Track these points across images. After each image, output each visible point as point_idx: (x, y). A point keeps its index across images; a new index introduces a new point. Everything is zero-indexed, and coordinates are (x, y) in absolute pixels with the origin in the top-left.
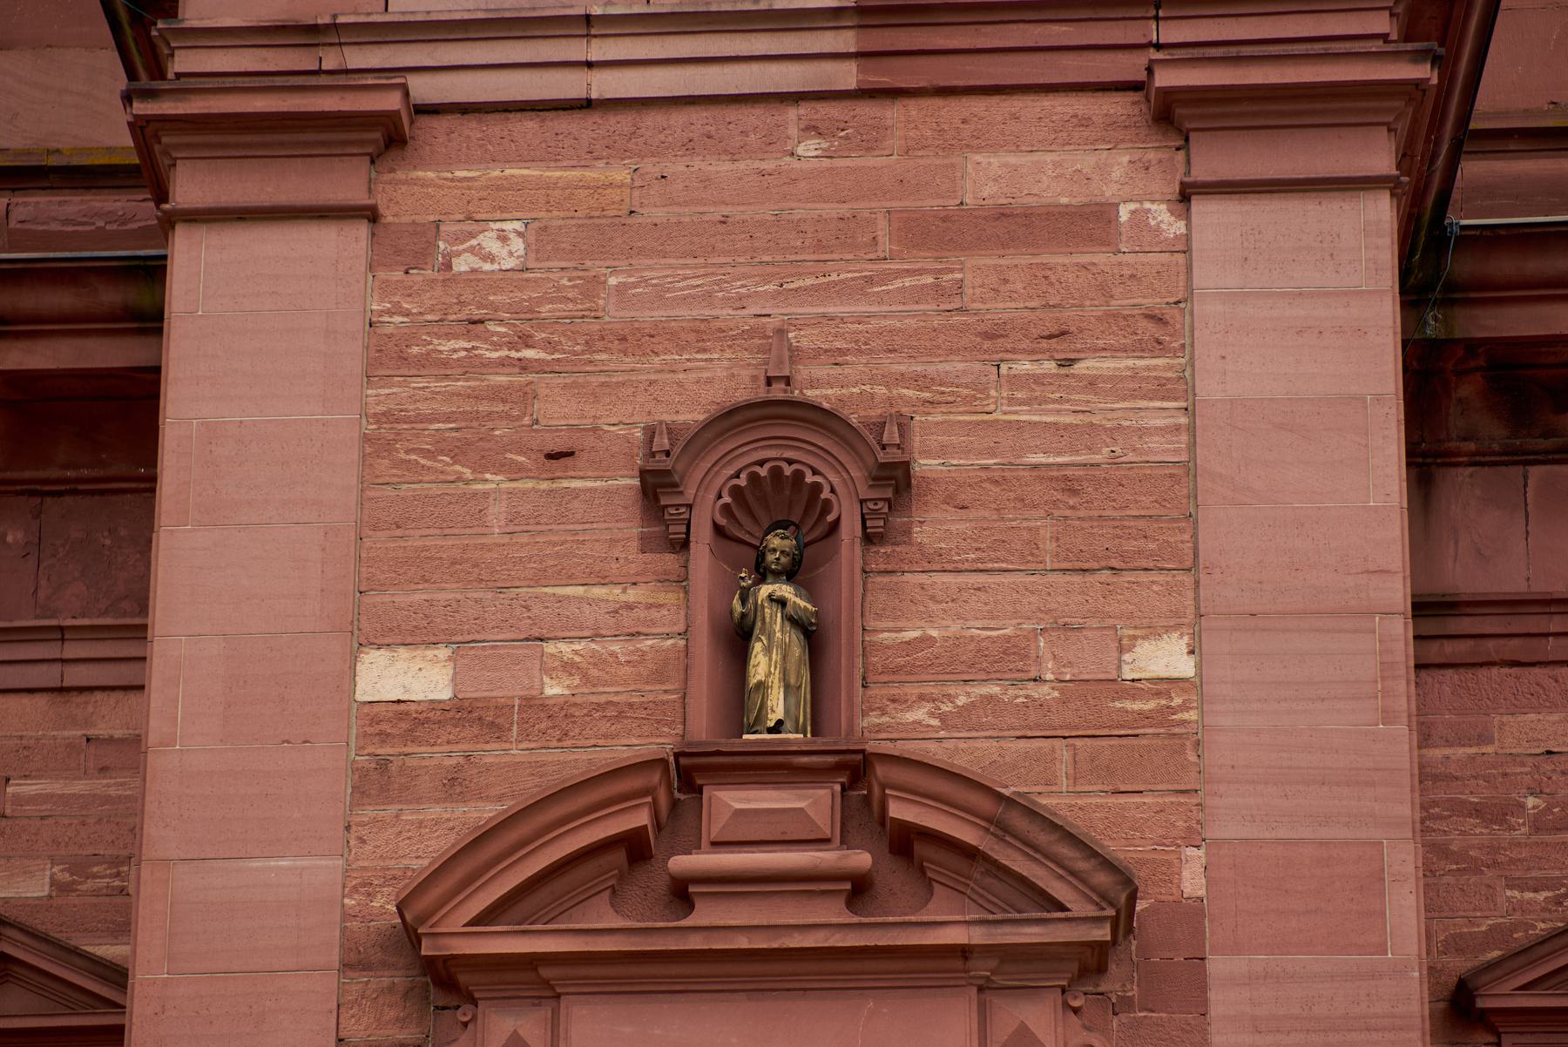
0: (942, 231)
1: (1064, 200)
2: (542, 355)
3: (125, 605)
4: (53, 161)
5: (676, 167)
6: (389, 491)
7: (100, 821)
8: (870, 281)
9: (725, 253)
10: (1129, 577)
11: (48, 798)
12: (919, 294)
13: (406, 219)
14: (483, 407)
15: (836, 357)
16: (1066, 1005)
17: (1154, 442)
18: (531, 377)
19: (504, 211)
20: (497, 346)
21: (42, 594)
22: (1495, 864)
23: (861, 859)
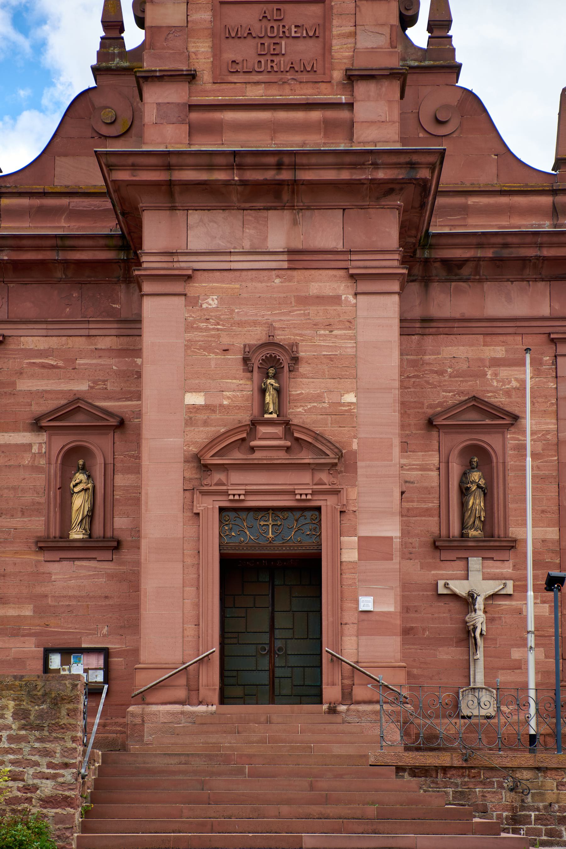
0: (305, 301)
1: (331, 294)
2: (222, 327)
3: (104, 314)
4: (79, 191)
5: (249, 285)
6: (190, 358)
7: (99, 370)
8: (290, 312)
9: (260, 305)
10: (343, 380)
11: (86, 364)
12: (300, 315)
13: (192, 295)
14: (210, 339)
15: (283, 329)
16: (329, 473)
17: (349, 350)
18: (220, 332)
19: (213, 294)
20: (212, 325)
21: (83, 311)
22: (440, 386)
23: (288, 443)
